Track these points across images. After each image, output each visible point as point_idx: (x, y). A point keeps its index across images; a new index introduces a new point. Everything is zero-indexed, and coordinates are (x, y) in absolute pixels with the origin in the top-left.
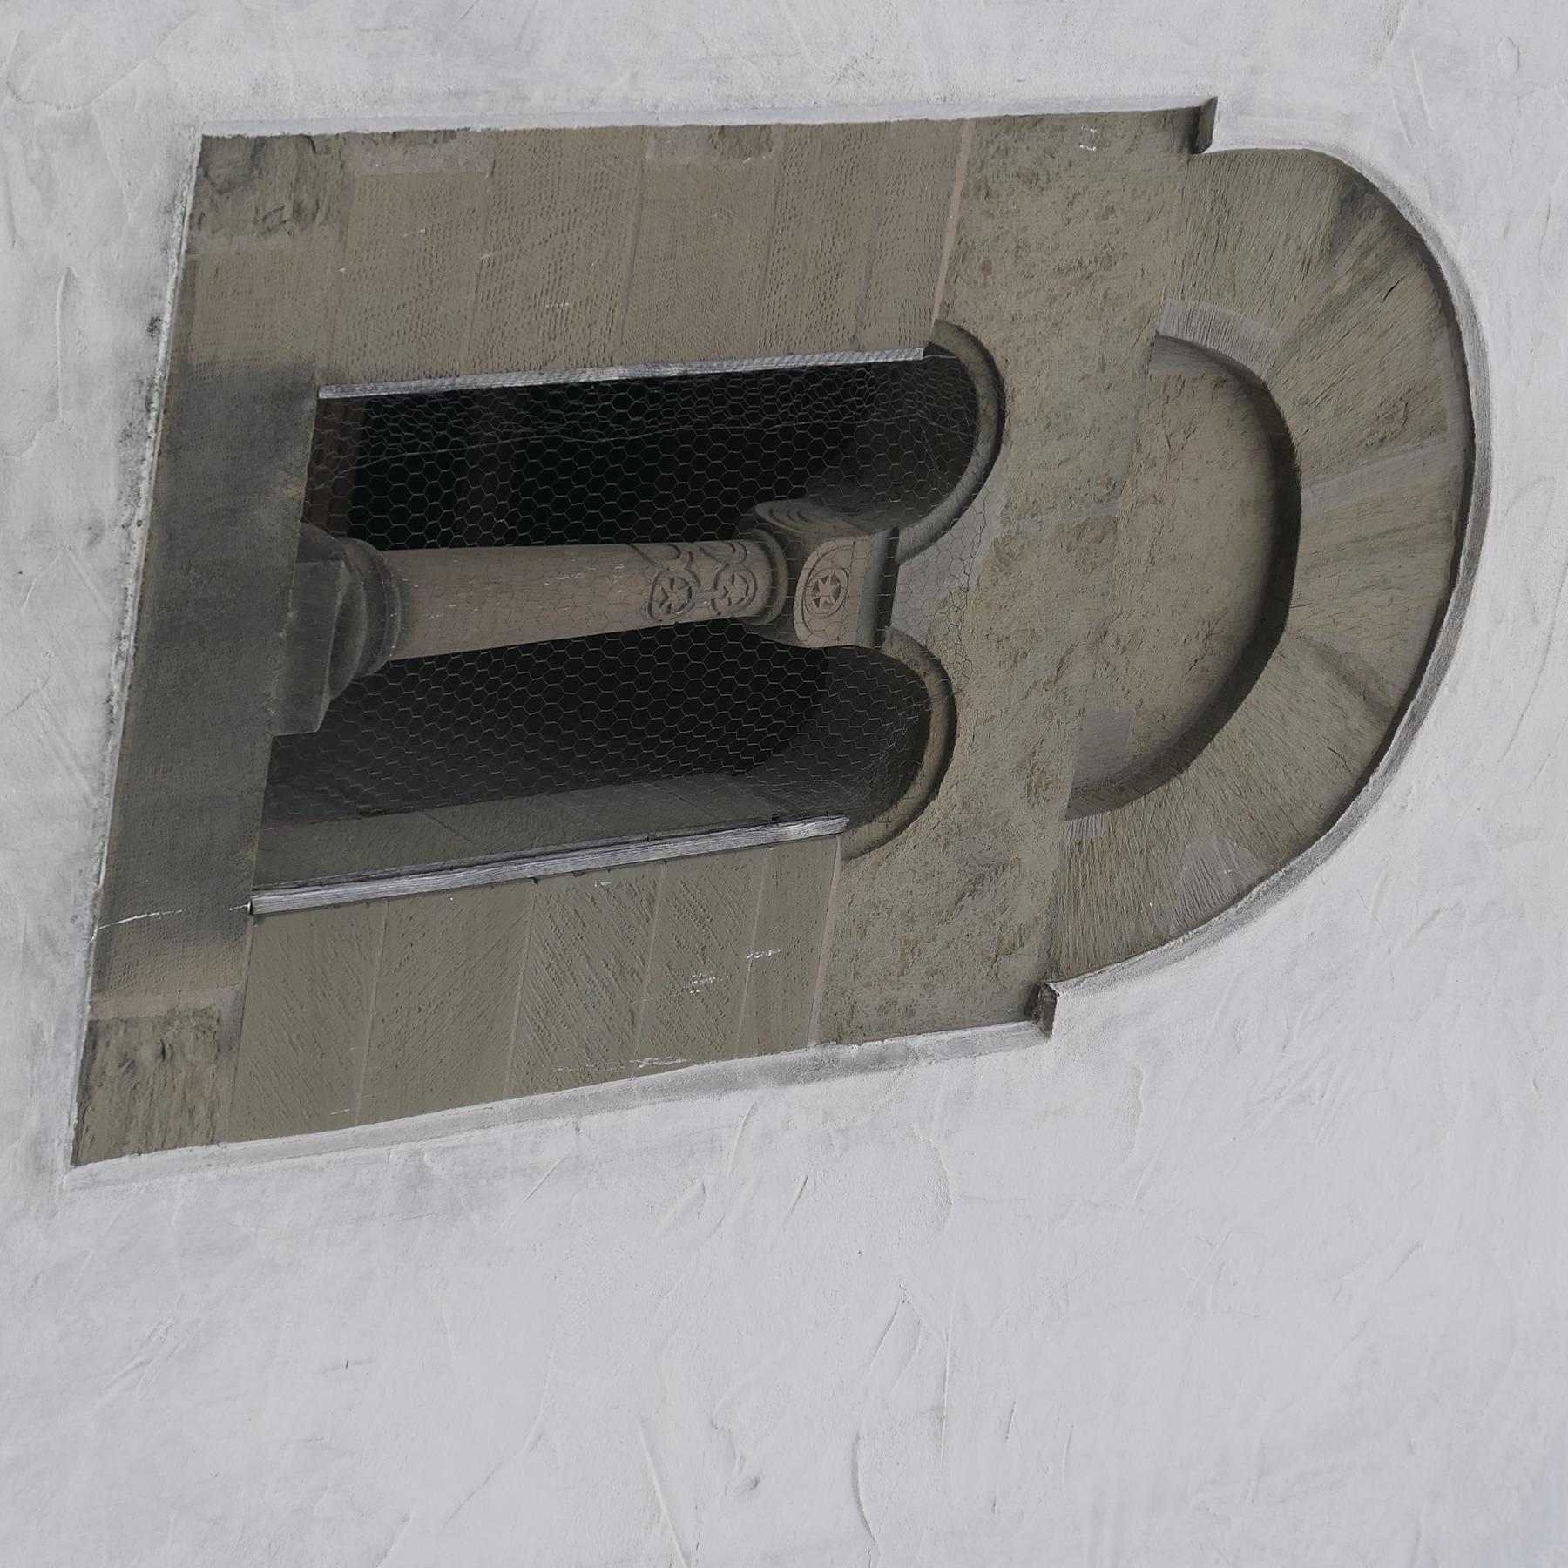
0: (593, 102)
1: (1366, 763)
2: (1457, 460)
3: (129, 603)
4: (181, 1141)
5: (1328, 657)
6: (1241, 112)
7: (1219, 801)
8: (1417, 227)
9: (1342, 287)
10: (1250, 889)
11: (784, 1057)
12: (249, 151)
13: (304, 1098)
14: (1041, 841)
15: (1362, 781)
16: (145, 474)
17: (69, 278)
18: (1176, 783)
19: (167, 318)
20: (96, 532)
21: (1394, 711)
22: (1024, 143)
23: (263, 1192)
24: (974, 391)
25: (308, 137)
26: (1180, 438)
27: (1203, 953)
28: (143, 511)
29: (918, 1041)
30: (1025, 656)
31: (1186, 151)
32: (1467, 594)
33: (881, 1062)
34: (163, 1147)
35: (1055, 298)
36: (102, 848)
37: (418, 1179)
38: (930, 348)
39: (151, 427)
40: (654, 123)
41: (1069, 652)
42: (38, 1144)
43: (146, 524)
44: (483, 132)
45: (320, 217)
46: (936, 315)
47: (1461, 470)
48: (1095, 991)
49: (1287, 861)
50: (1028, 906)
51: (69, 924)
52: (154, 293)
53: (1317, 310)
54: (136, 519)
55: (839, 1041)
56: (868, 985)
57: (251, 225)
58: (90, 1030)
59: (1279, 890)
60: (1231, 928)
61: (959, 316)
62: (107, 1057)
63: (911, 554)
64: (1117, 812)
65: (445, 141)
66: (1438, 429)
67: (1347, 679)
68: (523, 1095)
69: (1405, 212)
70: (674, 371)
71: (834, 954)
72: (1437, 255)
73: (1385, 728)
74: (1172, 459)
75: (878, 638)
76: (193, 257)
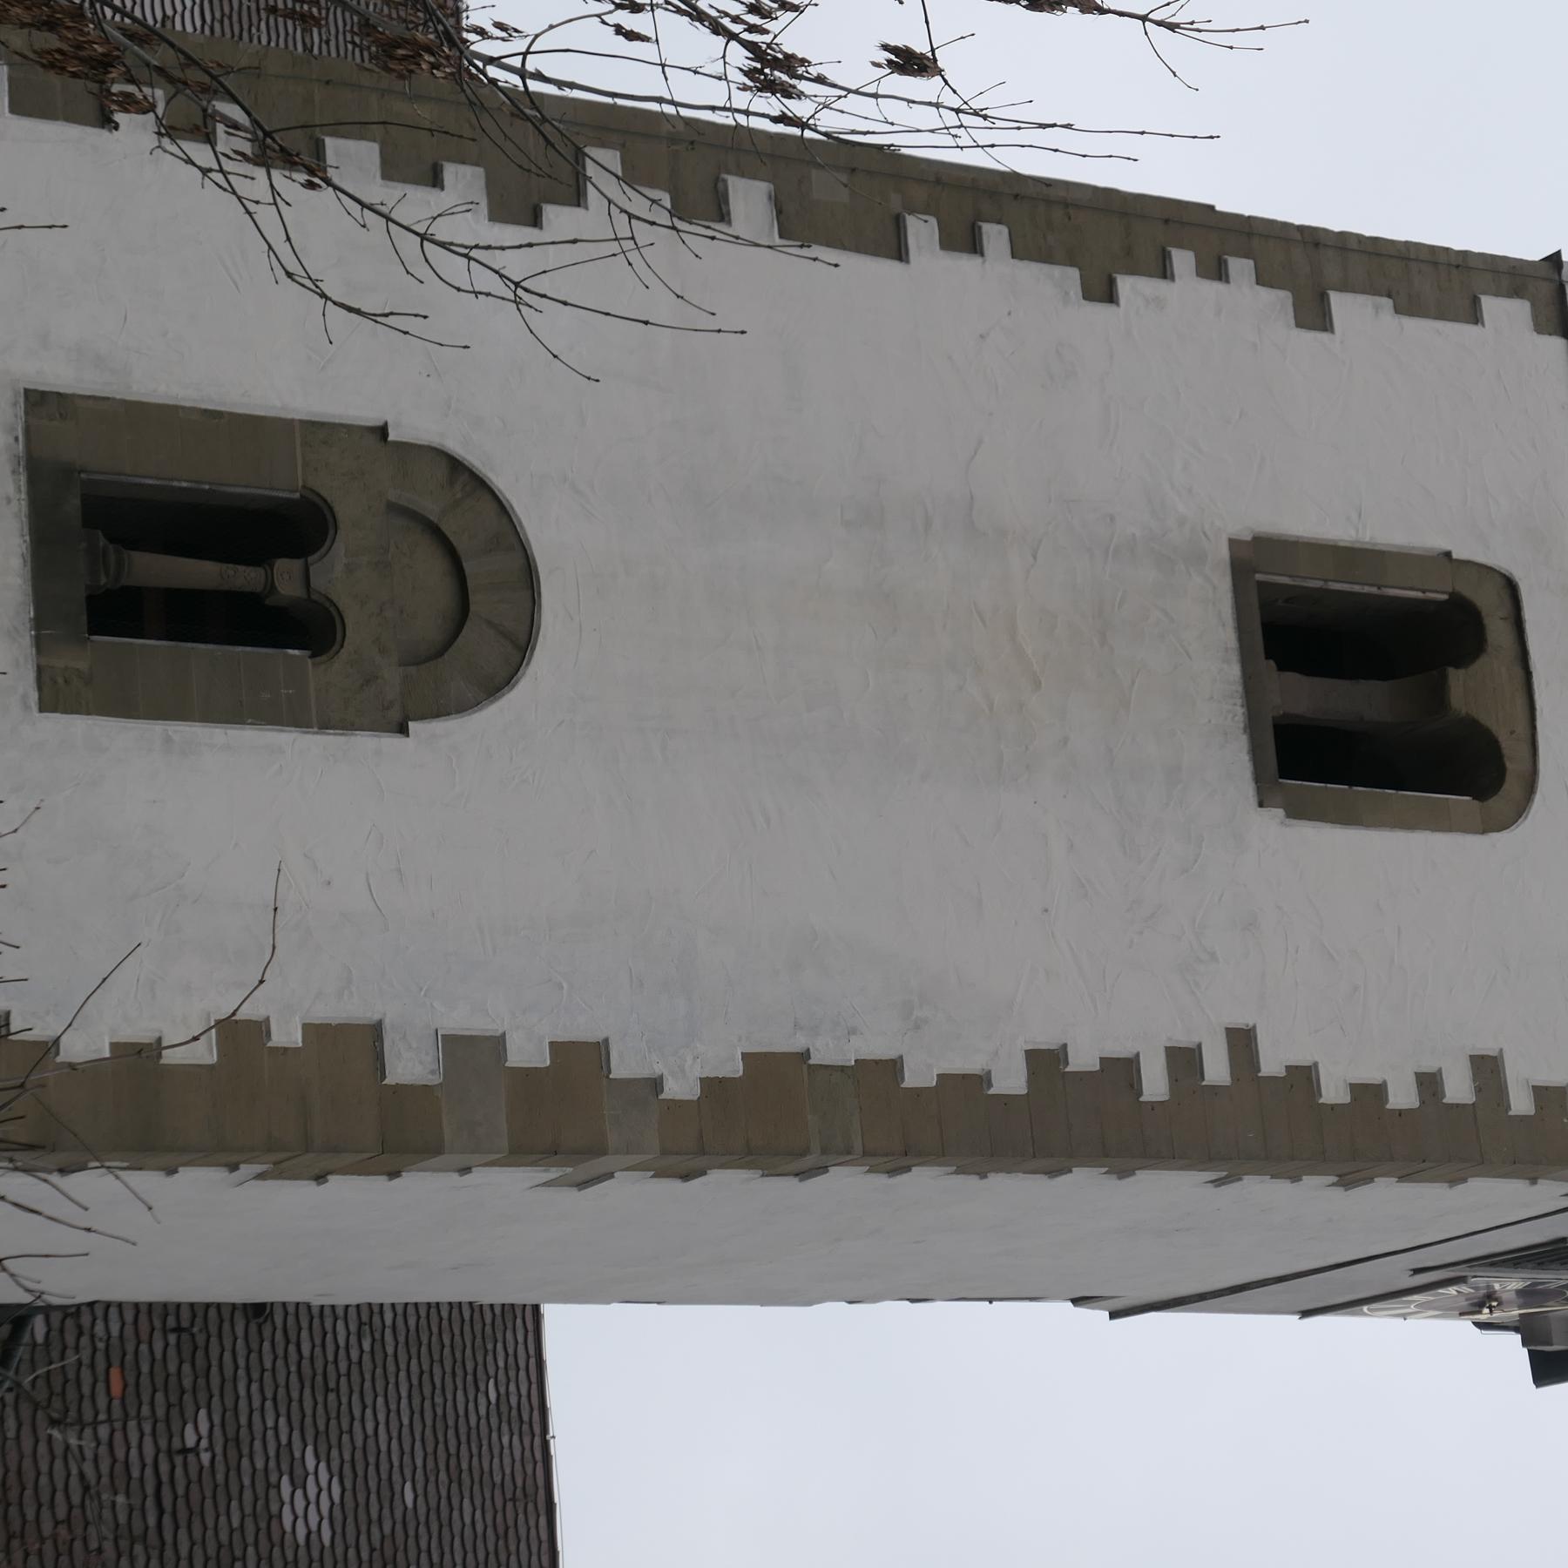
9: (459, 496)
20: (9, 501)
28: (23, 496)
37: (168, 740)
59: (492, 702)
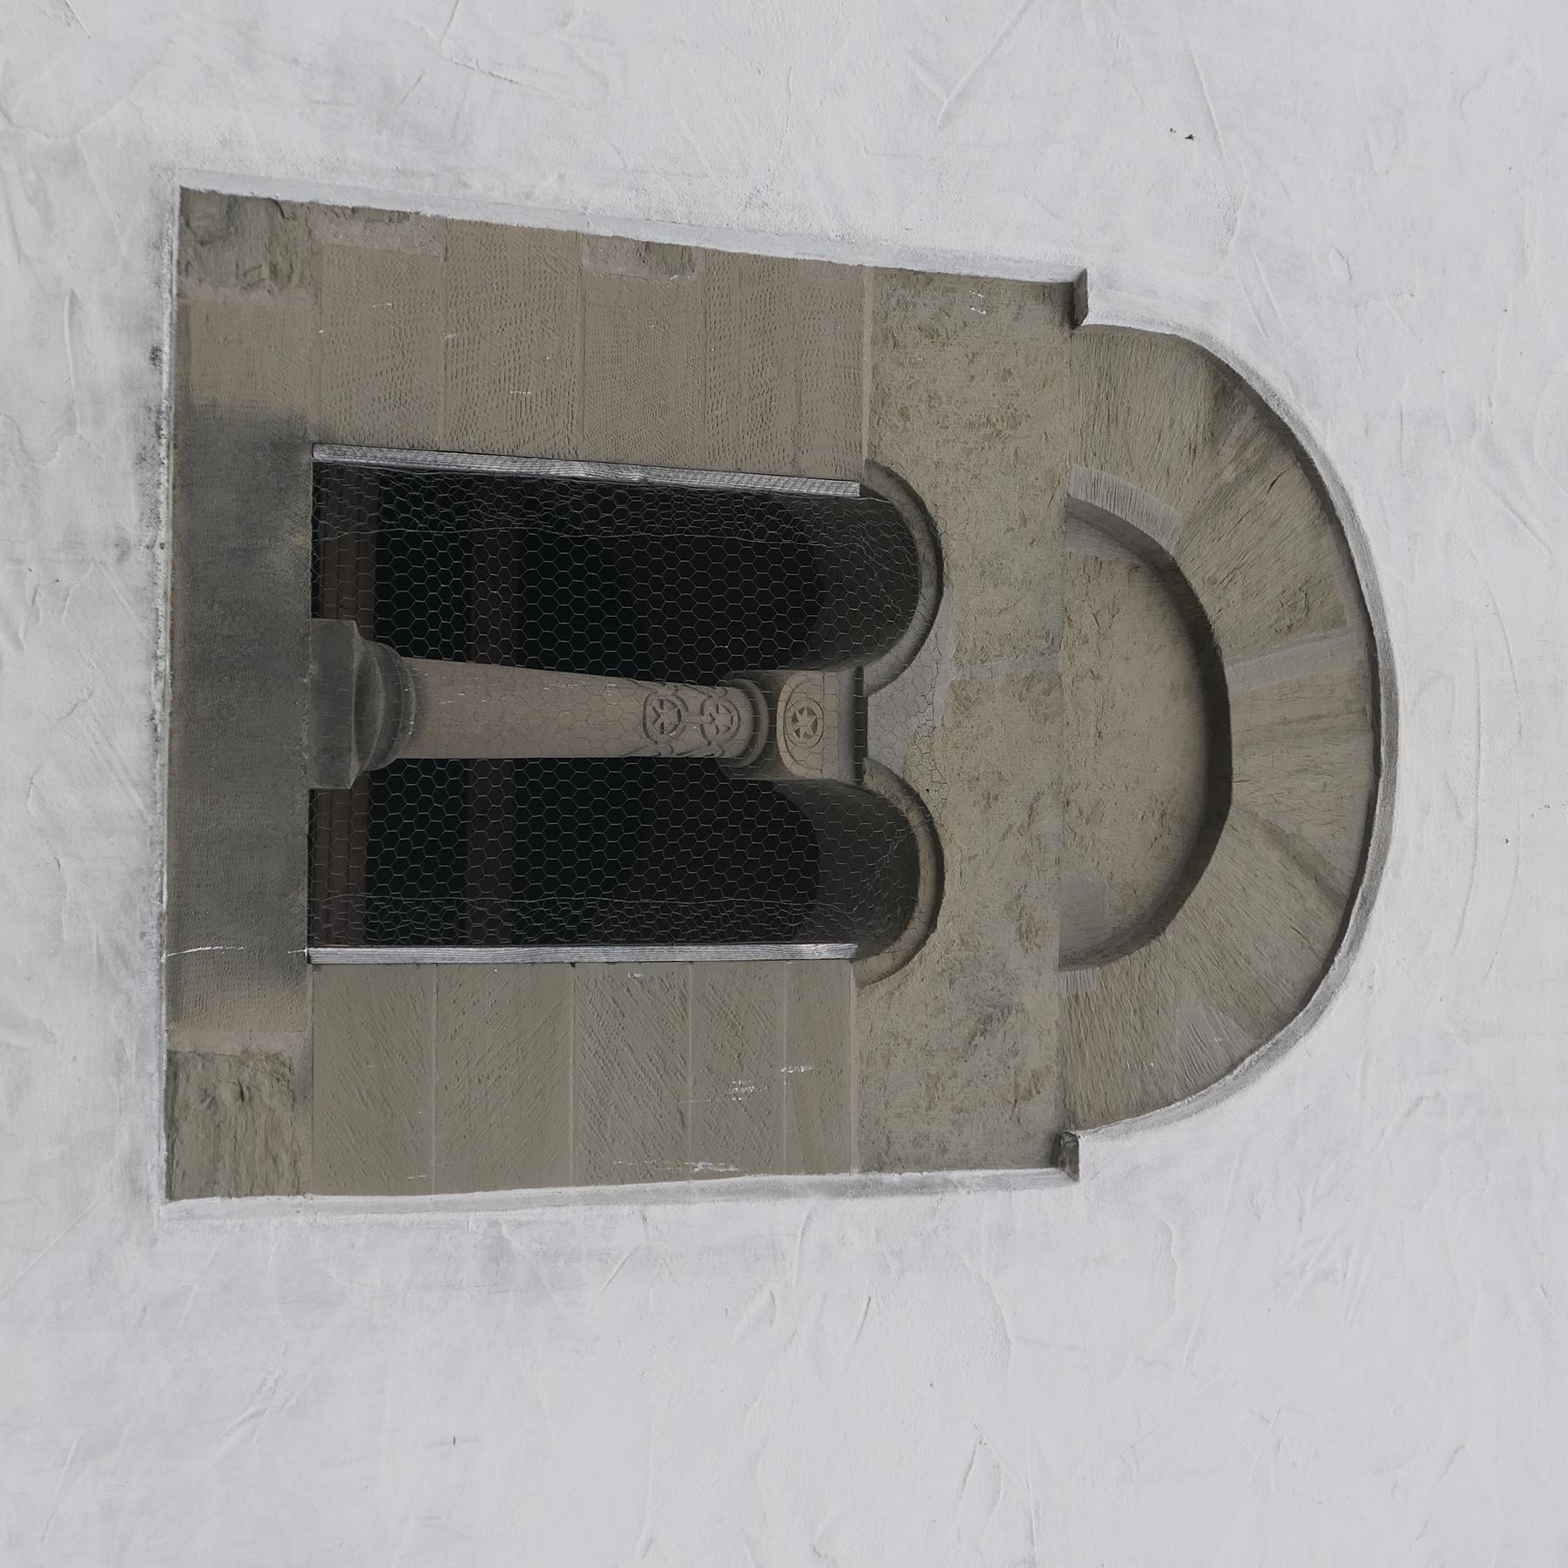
0: (528, 196)
1: (1329, 946)
2: (1361, 654)
3: (161, 624)
4: (268, 1190)
5: (1274, 834)
6: (1111, 286)
7: (1199, 970)
8: (1286, 420)
9: (1228, 475)
10: (1242, 1059)
11: (830, 1177)
12: (225, 208)
13: (380, 1154)
14: (1042, 992)
15: (1328, 962)
16: (162, 498)
17: (74, 299)
18: (1155, 945)
19: (166, 349)
20: (123, 550)
21: (1346, 895)
22: (918, 297)
23: (353, 1246)
24: (911, 536)
25: (276, 202)
26: (1105, 618)
27: (1208, 1113)
28: (164, 535)
29: (956, 1175)
30: (996, 798)
31: (1067, 327)
32: (1392, 782)
33: (922, 1188)
34: (251, 1193)
35: (971, 451)
36: (160, 883)
37: (499, 1252)
38: (865, 491)
39: (163, 454)
40: (586, 230)
41: (1037, 799)
42: (132, 1164)
43: (168, 547)
44: (434, 218)
45: (295, 278)
46: (865, 456)
47: (1366, 665)
48: (1113, 1138)
49: (1272, 1035)
50: (1038, 1053)
51: (138, 940)
52: (151, 324)
53: (1210, 494)
54: (159, 541)
55: (881, 1169)
56: (899, 1115)
57: (233, 280)
58: (169, 1060)
59: (1269, 1059)
60: (1230, 1092)
61: (887, 457)
62: (189, 1092)
63: (876, 689)
64: (1105, 968)
65: (400, 221)
66: (1338, 622)
67: (1297, 859)
68: (587, 1184)
69: (1272, 404)
70: (635, 476)
71: (864, 1080)
72: (1309, 449)
73: (1340, 914)
74: (1102, 636)
75: (858, 772)
76: (184, 301)
